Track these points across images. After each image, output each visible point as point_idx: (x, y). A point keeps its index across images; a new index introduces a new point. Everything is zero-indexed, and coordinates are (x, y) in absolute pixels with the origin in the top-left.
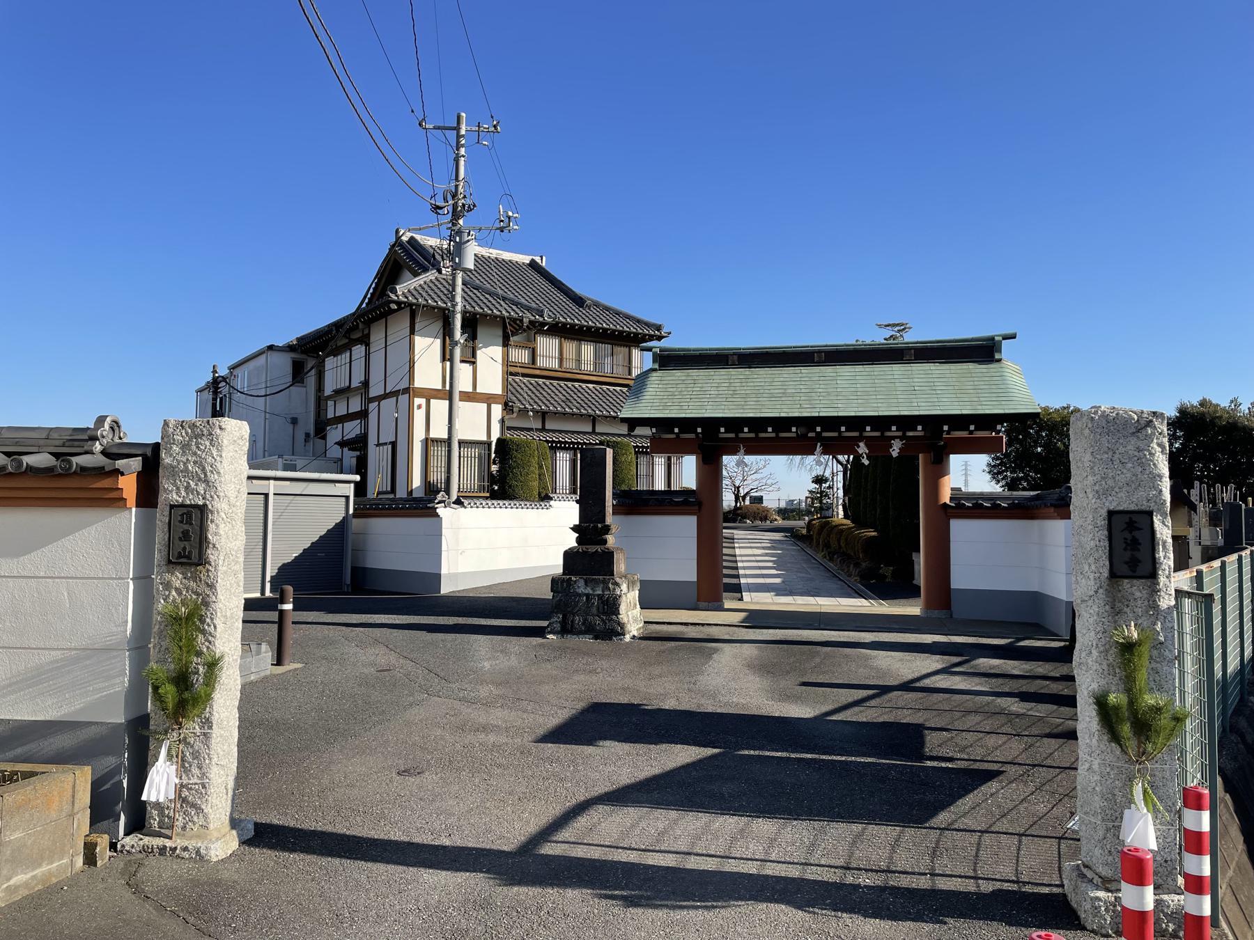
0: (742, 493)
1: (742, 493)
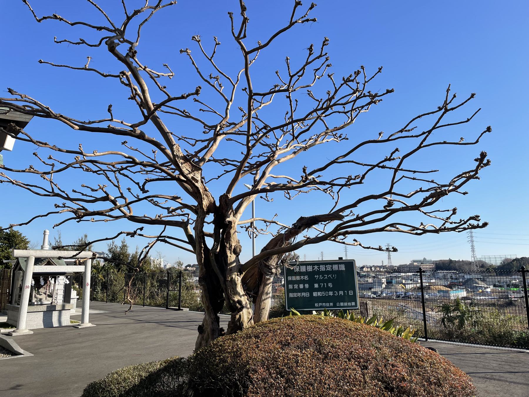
0: (247, 247)
1: (247, 247)
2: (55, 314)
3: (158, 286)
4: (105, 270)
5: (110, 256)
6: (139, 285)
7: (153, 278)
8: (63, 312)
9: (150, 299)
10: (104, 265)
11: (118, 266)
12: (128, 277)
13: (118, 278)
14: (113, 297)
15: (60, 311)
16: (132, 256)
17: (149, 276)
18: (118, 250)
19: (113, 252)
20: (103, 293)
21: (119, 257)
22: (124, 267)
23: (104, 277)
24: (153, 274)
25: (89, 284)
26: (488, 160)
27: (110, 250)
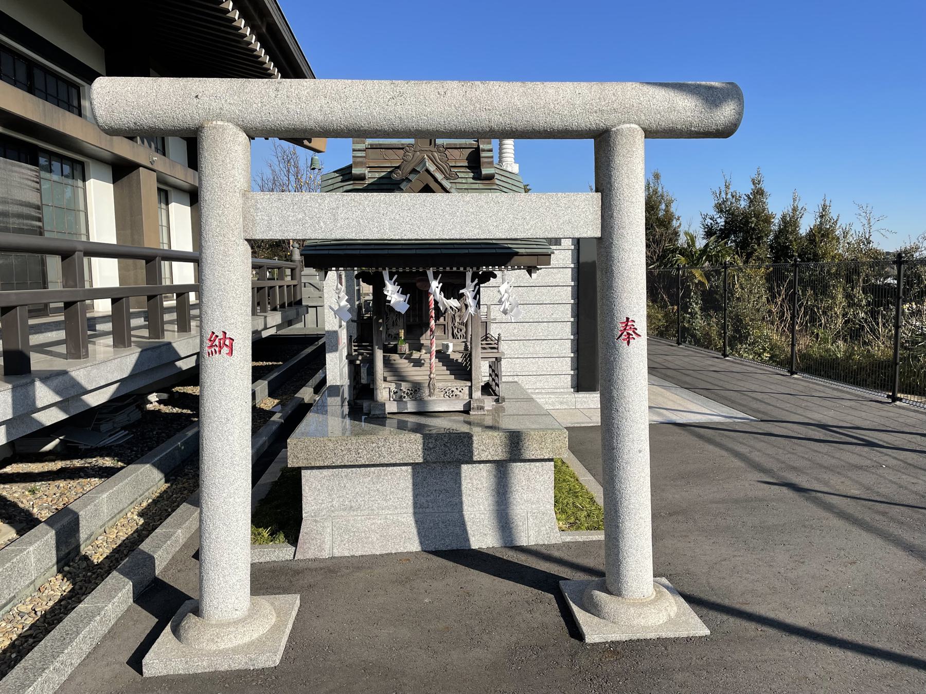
2: (476, 484)
3: (868, 304)
4: (709, 259)
5: (721, 222)
6: (808, 298)
7: (849, 280)
8: (518, 470)
9: (845, 341)
10: (707, 245)
11: (745, 249)
12: (774, 279)
13: (750, 286)
14: (736, 330)
15: (501, 470)
16: (784, 218)
17: (837, 275)
18: (743, 204)
19: (729, 212)
20: (707, 316)
21: (747, 222)
22: (763, 252)
23: (707, 275)
24: (850, 272)
25: (642, 325)
26: (686, 233)
27: (720, 208)
